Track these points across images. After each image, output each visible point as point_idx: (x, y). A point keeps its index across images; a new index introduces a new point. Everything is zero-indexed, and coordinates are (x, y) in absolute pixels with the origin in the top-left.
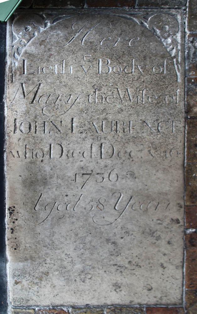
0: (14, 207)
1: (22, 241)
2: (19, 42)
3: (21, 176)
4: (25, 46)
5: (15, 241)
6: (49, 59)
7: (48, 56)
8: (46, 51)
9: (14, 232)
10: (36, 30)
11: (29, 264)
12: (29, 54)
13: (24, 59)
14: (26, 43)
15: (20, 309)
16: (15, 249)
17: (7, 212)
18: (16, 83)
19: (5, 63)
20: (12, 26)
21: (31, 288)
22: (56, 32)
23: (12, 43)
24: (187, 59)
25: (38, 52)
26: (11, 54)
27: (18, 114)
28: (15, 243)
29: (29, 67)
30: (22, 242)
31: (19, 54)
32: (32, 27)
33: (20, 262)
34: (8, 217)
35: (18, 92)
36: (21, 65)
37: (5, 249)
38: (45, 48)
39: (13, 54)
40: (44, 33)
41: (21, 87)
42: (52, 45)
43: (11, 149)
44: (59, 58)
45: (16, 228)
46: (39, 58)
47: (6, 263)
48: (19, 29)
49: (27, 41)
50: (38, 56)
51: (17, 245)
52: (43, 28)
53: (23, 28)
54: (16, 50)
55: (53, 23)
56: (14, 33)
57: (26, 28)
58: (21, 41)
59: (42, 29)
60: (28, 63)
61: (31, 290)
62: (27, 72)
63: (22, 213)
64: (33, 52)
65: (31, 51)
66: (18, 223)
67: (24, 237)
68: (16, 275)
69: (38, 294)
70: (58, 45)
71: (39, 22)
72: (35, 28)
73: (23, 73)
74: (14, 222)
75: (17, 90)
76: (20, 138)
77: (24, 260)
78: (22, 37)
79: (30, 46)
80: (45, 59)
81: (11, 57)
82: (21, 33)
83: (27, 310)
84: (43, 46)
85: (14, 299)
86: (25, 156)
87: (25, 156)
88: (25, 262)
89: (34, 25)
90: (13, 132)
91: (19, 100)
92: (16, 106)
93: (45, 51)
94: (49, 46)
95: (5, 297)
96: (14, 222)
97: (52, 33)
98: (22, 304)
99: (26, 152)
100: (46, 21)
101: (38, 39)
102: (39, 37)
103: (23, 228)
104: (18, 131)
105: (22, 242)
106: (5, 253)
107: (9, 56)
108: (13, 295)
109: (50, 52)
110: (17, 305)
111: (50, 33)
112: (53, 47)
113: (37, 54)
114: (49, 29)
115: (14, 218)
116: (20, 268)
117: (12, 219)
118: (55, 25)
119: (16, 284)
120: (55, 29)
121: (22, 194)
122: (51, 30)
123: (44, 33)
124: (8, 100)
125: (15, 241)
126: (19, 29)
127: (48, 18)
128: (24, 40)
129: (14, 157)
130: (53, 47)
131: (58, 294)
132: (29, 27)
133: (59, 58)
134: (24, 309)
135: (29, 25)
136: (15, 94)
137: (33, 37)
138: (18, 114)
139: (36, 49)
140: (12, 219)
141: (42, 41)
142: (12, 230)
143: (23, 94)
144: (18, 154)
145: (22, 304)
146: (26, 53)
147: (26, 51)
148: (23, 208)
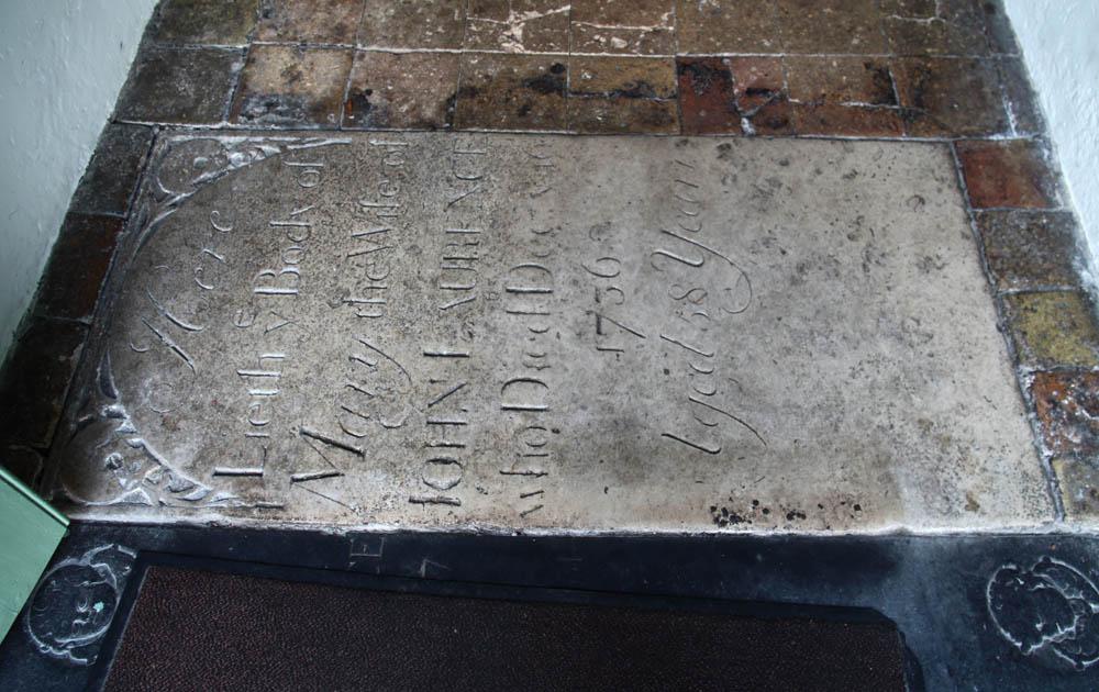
0: (714, 509)
3: (606, 489)
16: (857, 508)
17: (730, 530)
18: (288, 496)
20: (89, 506)
30: (829, 489)
31: (191, 488)
34: (749, 526)
39: (187, 505)
43: (514, 515)
45: (785, 506)
51: (843, 503)
54: (177, 495)
60: (229, 462)
63: (731, 487)
68: (947, 506)
74: (766, 511)
75: (312, 495)
78: (135, 477)
81: (197, 509)
82: (123, 481)
86: (538, 476)
87: (538, 476)
90: (455, 509)
96: (766, 511)
99: (527, 474)
100: (104, 414)
103: (782, 485)
104: (452, 495)
106: (876, 537)
107: (190, 514)
109: (206, 406)
115: (751, 510)
116: (920, 496)
117: (754, 515)
121: (667, 486)
127: (93, 409)
128: (149, 473)
129: (541, 506)
134: (1057, 486)
138: (394, 493)
140: (754, 515)
144: (531, 495)
147: (185, 468)
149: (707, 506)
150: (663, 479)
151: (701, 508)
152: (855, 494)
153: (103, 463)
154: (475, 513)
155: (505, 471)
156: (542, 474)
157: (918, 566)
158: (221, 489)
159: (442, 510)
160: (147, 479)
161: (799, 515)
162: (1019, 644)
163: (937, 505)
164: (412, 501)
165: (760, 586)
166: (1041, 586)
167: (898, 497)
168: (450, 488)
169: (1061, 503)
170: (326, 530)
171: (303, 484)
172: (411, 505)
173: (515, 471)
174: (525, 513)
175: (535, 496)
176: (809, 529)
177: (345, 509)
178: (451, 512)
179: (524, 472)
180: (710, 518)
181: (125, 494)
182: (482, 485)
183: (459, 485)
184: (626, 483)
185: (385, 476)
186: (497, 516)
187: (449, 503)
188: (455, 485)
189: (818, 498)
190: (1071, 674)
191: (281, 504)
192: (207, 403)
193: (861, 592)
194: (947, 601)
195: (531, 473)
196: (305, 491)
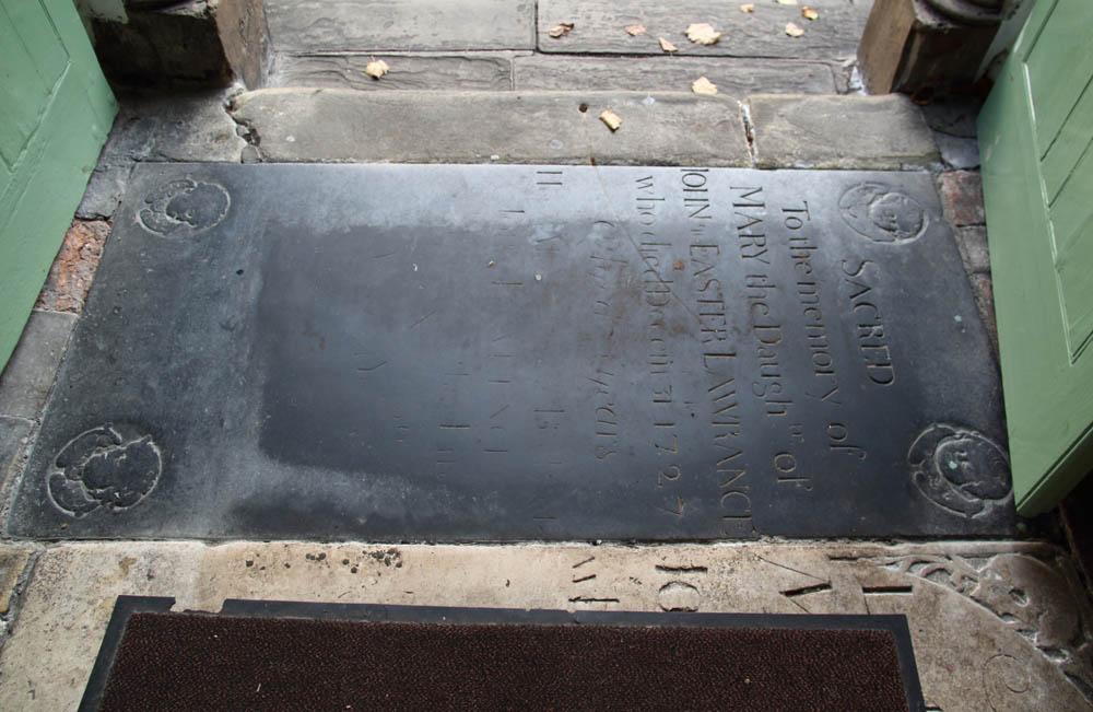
0: (399, 565)
1: (276, 583)
2: (967, 573)
3: (508, 585)
4: (961, 591)
5: (279, 564)
6: (933, 664)
7: (941, 659)
8: (957, 652)
9: (310, 563)
10: (1026, 621)
11: (184, 602)
12: (935, 602)
13: (914, 589)
14: (972, 594)
15: (24, 573)
16: (249, 564)
17: (385, 547)
18: (828, 570)
19: (888, 539)
20: (1016, 552)
21: (92, 607)
22: (1036, 683)
23: (958, 555)
24: (994, 505)
25: (948, 629)
26: (920, 554)
27: (725, 576)
28: (271, 562)
29: (890, 603)
30: (273, 584)
31: (928, 574)
32: (1028, 608)
33: (198, 576)
34: (365, 549)
35: (798, 575)
36: (891, 579)
37: (255, 540)
38: (967, 649)
39: (924, 557)
40: (1022, 646)
41: (817, 584)
42: (984, 670)
43: (601, 558)
44: (944, 696)
45: (325, 567)
46: (928, 632)
47: (205, 539)
48: (1012, 572)
49: (977, 597)
50: (934, 627)
51: (263, 568)
52: (1038, 641)
53: (1017, 583)
54: (938, 566)
55: (1066, 673)
56: (993, 559)
57: (1019, 592)
58: (972, 579)
59: (1035, 640)
60: (903, 602)
61: (83, 606)
62: (871, 598)
63: (377, 586)
64: (944, 614)
65: (948, 607)
66: (340, 573)
67: (286, 591)
68: (154, 563)
69: (61, 630)
70: (991, 689)
71: (1053, 628)
72: (1030, 616)
73: (867, 586)
74: (346, 562)
75: (806, 571)
76: (640, 583)
77: (206, 586)
78: (989, 581)
79: (962, 603)
80: (931, 650)
81: (911, 553)
82: (998, 578)
83: (11, 592)
84: (973, 642)
85: (67, 553)
86: (578, 599)
87: (578, 599)
88: (198, 590)
89: (1041, 613)
90: (661, 563)
91: (770, 578)
92: (749, 570)
93: (956, 649)
94: (978, 661)
95: (84, 532)
96: (346, 562)
97: (1028, 669)
98: (40, 578)
99: (591, 600)
100: (1065, 652)
101: (996, 628)
102: (1002, 629)
103: (323, 588)
104: (666, 577)
105: (273, 584)
106: (239, 539)
107: (915, 548)
108: (83, 551)
109: (958, 666)
110: (41, 562)
111: (1026, 663)
112: (978, 674)
113: (941, 625)
114: (1040, 659)
115: (361, 564)
116: (179, 575)
117: (359, 558)
118: (1061, 681)
119: (120, 563)
120: (1048, 679)
121: (444, 589)
122: (1038, 666)
123: (1022, 646)
124: (768, 547)
125: (279, 564)
126: (1012, 572)
127: (1081, 657)
128: (978, 587)
129: (575, 567)
130: (978, 674)
131: (34, 698)
132: (1028, 600)
133: (944, 696)
134: (19, 585)
135: (1033, 601)
136: (791, 565)
137: (997, 613)
138: (725, 576)
139: (959, 621)
140: (359, 558)
141: (992, 640)
142: (203, 76)
143: (796, 588)
144: (585, 579)
145: (40, 578)
146: (937, 593)
147: (943, 593)
148: (394, 591)
149: (405, 568)
150: (447, 596)
151: (412, 567)
152: (248, 578)
153: (1030, 595)
154: (640, 559)
155: (615, 603)
156: (574, 600)
157: (211, 511)
158: (898, 574)
159: (672, 561)
160: (976, 581)
161: (313, 558)
162: (151, 443)
163: (164, 565)
164: (703, 569)
165: (368, 495)
166: (99, 491)
167: (202, 574)
168: (668, 584)
169: (26, 567)
170: (781, 541)
171: (817, 582)
172: (704, 565)
173: (604, 603)
174: (590, 560)
175: (580, 577)
176: (301, 547)
177: (769, 558)
178: (664, 559)
179: (593, 602)
180: (404, 557)
181: (989, 565)
182: (637, 587)
183: (660, 586)
184: (487, 591)
185: (737, 593)
186: (618, 557)
187: (668, 569)
188: (664, 587)
189: (287, 575)
190: (117, 422)
191: (832, 561)
192: (958, 670)
193: (275, 487)
194: (197, 478)
195: (586, 601)
196: (813, 574)
